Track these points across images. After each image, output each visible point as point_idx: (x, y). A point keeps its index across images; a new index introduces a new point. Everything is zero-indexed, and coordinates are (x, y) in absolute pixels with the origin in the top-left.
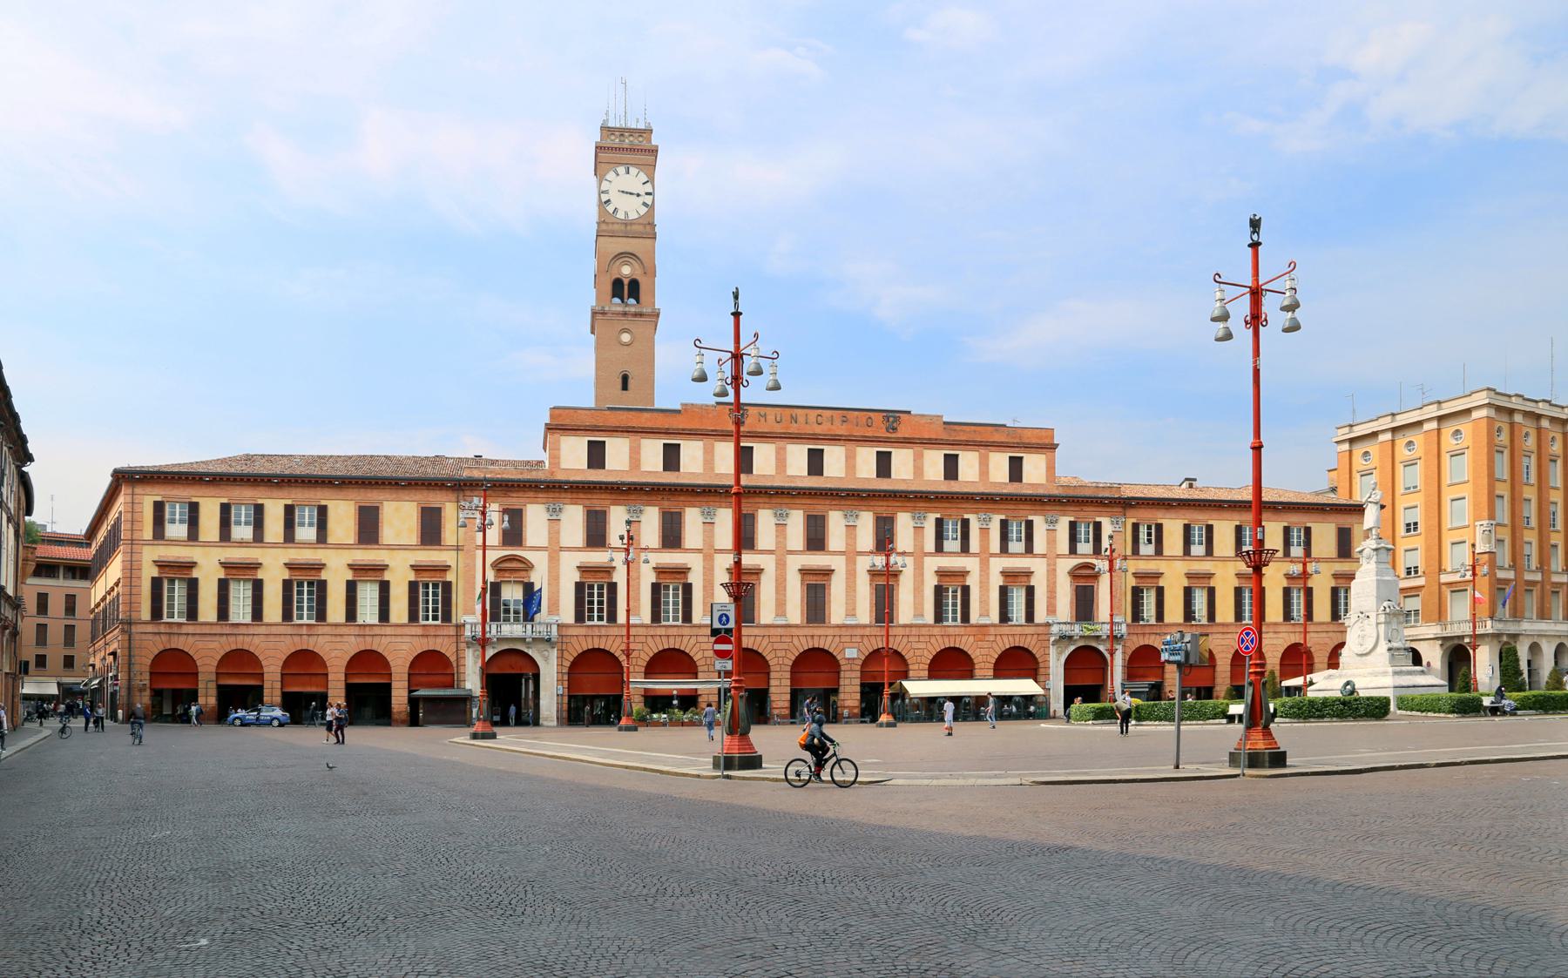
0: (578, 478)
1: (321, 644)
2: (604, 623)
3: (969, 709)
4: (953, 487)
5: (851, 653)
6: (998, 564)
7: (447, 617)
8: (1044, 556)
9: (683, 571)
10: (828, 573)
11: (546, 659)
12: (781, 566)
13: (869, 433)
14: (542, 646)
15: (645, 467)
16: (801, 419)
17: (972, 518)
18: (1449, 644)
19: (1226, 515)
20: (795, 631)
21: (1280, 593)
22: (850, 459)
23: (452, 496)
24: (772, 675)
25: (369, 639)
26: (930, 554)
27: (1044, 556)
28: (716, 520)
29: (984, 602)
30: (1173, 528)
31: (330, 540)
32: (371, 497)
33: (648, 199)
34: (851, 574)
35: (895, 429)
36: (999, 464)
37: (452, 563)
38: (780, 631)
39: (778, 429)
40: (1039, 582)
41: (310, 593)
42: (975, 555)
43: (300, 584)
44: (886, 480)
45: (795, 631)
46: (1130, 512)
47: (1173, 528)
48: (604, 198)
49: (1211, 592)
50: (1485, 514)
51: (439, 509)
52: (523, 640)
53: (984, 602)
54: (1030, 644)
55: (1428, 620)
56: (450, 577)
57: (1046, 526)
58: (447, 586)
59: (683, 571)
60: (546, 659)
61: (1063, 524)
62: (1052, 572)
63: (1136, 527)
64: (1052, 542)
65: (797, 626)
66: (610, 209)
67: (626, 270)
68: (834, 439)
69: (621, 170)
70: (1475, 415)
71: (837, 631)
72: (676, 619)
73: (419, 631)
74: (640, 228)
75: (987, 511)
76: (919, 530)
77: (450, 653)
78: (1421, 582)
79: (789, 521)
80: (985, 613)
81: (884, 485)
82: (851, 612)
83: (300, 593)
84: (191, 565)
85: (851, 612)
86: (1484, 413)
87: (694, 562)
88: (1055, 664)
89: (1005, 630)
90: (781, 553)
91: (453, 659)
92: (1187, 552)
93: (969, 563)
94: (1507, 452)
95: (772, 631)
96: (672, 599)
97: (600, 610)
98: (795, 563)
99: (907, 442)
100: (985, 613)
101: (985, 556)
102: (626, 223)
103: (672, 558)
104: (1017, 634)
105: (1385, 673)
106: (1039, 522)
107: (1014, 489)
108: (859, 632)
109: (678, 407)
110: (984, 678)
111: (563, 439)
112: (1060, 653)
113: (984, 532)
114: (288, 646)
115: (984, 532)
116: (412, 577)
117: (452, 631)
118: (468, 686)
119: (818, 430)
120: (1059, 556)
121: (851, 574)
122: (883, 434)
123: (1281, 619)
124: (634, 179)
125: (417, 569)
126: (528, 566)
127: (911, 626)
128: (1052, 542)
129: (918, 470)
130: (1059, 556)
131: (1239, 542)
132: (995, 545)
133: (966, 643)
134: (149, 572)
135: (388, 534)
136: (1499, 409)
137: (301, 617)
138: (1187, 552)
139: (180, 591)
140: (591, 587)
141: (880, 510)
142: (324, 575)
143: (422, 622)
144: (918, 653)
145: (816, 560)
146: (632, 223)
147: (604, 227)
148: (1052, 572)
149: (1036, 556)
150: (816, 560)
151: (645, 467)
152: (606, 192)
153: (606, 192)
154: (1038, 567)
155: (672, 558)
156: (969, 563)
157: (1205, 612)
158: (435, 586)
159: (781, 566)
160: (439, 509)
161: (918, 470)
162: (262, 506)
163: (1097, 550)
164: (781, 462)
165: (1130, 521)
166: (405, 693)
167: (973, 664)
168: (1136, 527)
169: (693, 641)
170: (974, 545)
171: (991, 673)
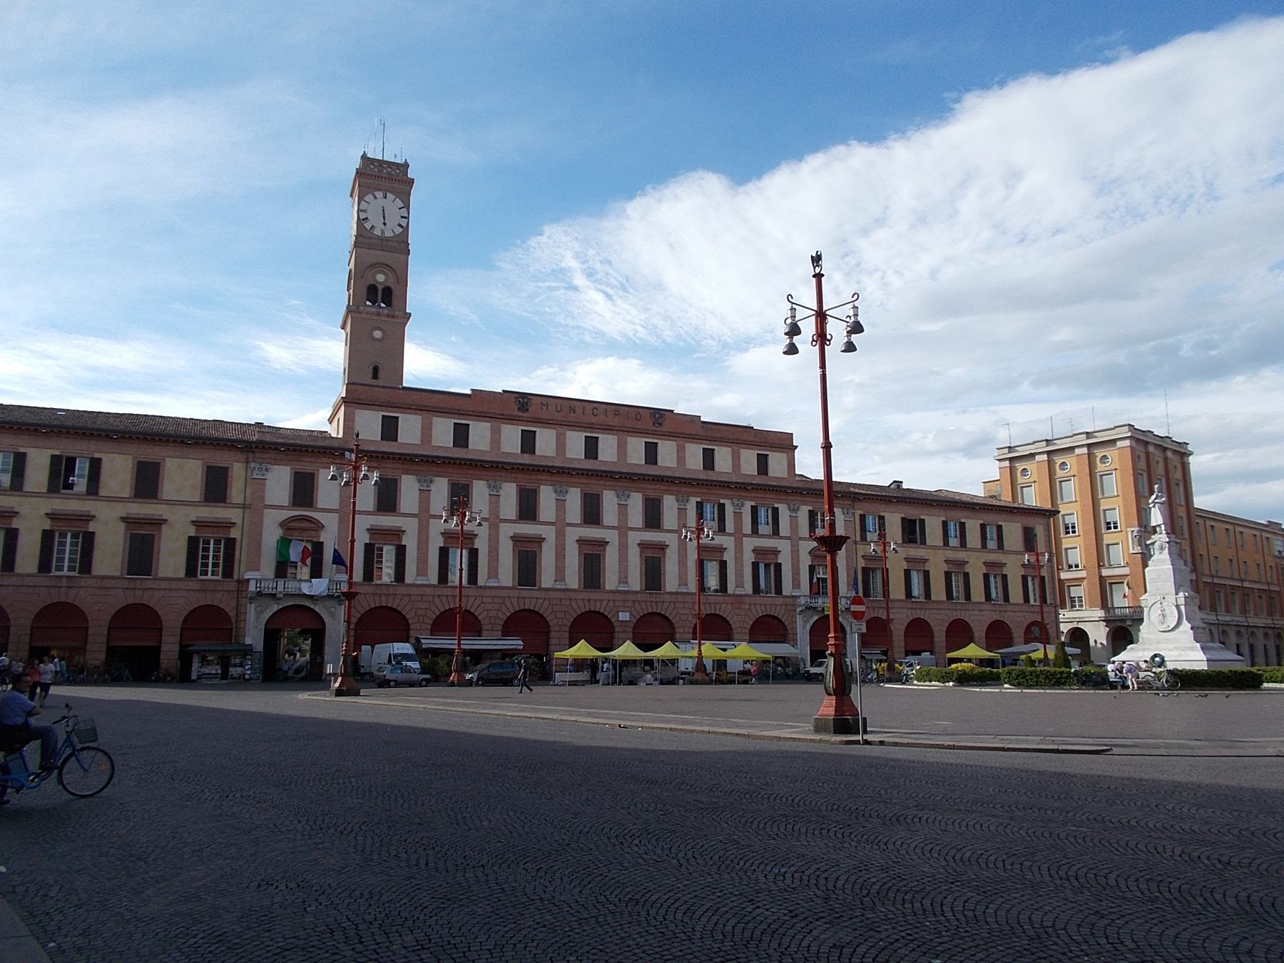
0: (372, 448)
1: (83, 596)
2: (219, 577)
3: (720, 674)
4: (710, 476)
5: (624, 616)
6: (750, 544)
7: (228, 572)
8: (787, 538)
9: (397, 533)
10: (603, 544)
11: (333, 615)
12: (560, 536)
13: (639, 425)
14: (329, 603)
15: (570, 454)
16: (579, 411)
17: (727, 503)
18: (1113, 625)
19: (935, 511)
20: (573, 595)
21: (38, 537)
22: (622, 448)
23: (240, 455)
24: (552, 634)
25: (139, 593)
26: (805, 539)
27: (787, 538)
28: (502, 493)
29: (739, 575)
30: (973, 526)
31: (102, 493)
32: (151, 453)
33: (404, 223)
34: (623, 547)
35: (660, 424)
36: (636, 448)
37: (238, 521)
38: (559, 595)
39: (559, 416)
40: (785, 560)
41: (74, 544)
42: (730, 535)
43: (63, 535)
44: (592, 461)
45: (573, 595)
46: (857, 505)
47: (973, 526)
48: (363, 216)
49: (926, 574)
50: (1136, 522)
51: (313, 475)
52: (311, 597)
53: (739, 575)
54: (779, 612)
55: (1092, 605)
56: (234, 534)
57: (788, 513)
58: (231, 543)
59: (397, 533)
60: (333, 615)
61: (804, 512)
62: (795, 552)
63: (863, 518)
64: (794, 526)
65: (574, 590)
66: (368, 226)
67: (381, 278)
68: (608, 429)
69: (379, 194)
70: (1119, 444)
71: (611, 596)
72: (71, 569)
73: (196, 586)
74: (395, 244)
75: (739, 498)
76: (682, 512)
77: (228, 606)
78: (1083, 574)
79: (433, 487)
80: (740, 584)
81: (651, 470)
82: (623, 579)
83: (62, 544)
84: (90, 518)
85: (623, 579)
86: (1127, 443)
87: (410, 528)
88: (802, 628)
89: (758, 599)
90: (623, 529)
91: (232, 614)
92: (984, 545)
93: (720, 540)
94: (1145, 475)
95: (552, 594)
96: (68, 548)
97: (215, 565)
98: (573, 534)
99: (671, 435)
100: (740, 584)
101: (738, 535)
102: (383, 239)
103: (386, 521)
104: (768, 604)
105: (1193, 649)
106: (783, 510)
107: (761, 480)
108: (632, 597)
109: (469, 392)
110: (1019, 644)
111: (357, 411)
112: (807, 621)
113: (738, 516)
114: (120, 598)
115: (738, 516)
116: (192, 532)
117: (233, 586)
118: (248, 641)
119: (593, 420)
120: (800, 539)
121: (623, 547)
122: (650, 426)
123: (983, 600)
124: (392, 203)
125: (198, 524)
126: (319, 526)
127: (677, 593)
128: (794, 526)
129: (681, 459)
130: (800, 539)
131: (812, 526)
132: (747, 528)
133: (725, 610)
134: (362, 538)
135: (168, 489)
136: (1138, 440)
137: (60, 568)
138: (984, 545)
139: (389, 553)
140: (207, 542)
141: (456, 478)
142: (92, 527)
143: (54, 573)
144: (684, 617)
145: (592, 533)
146: (388, 239)
147: (361, 239)
148: (795, 552)
149: (782, 538)
150: (592, 533)
151: (570, 454)
152: (365, 211)
153: (365, 211)
154: (784, 546)
155: (386, 521)
156: (726, 541)
157: (1001, 595)
158: (217, 542)
159: (560, 536)
160: (227, 468)
161: (681, 459)
162: (100, 460)
163: (722, 529)
164: (561, 445)
165: (694, 500)
166: (176, 648)
167: (731, 629)
168: (863, 518)
169: (478, 602)
170: (730, 526)
171: (747, 637)
